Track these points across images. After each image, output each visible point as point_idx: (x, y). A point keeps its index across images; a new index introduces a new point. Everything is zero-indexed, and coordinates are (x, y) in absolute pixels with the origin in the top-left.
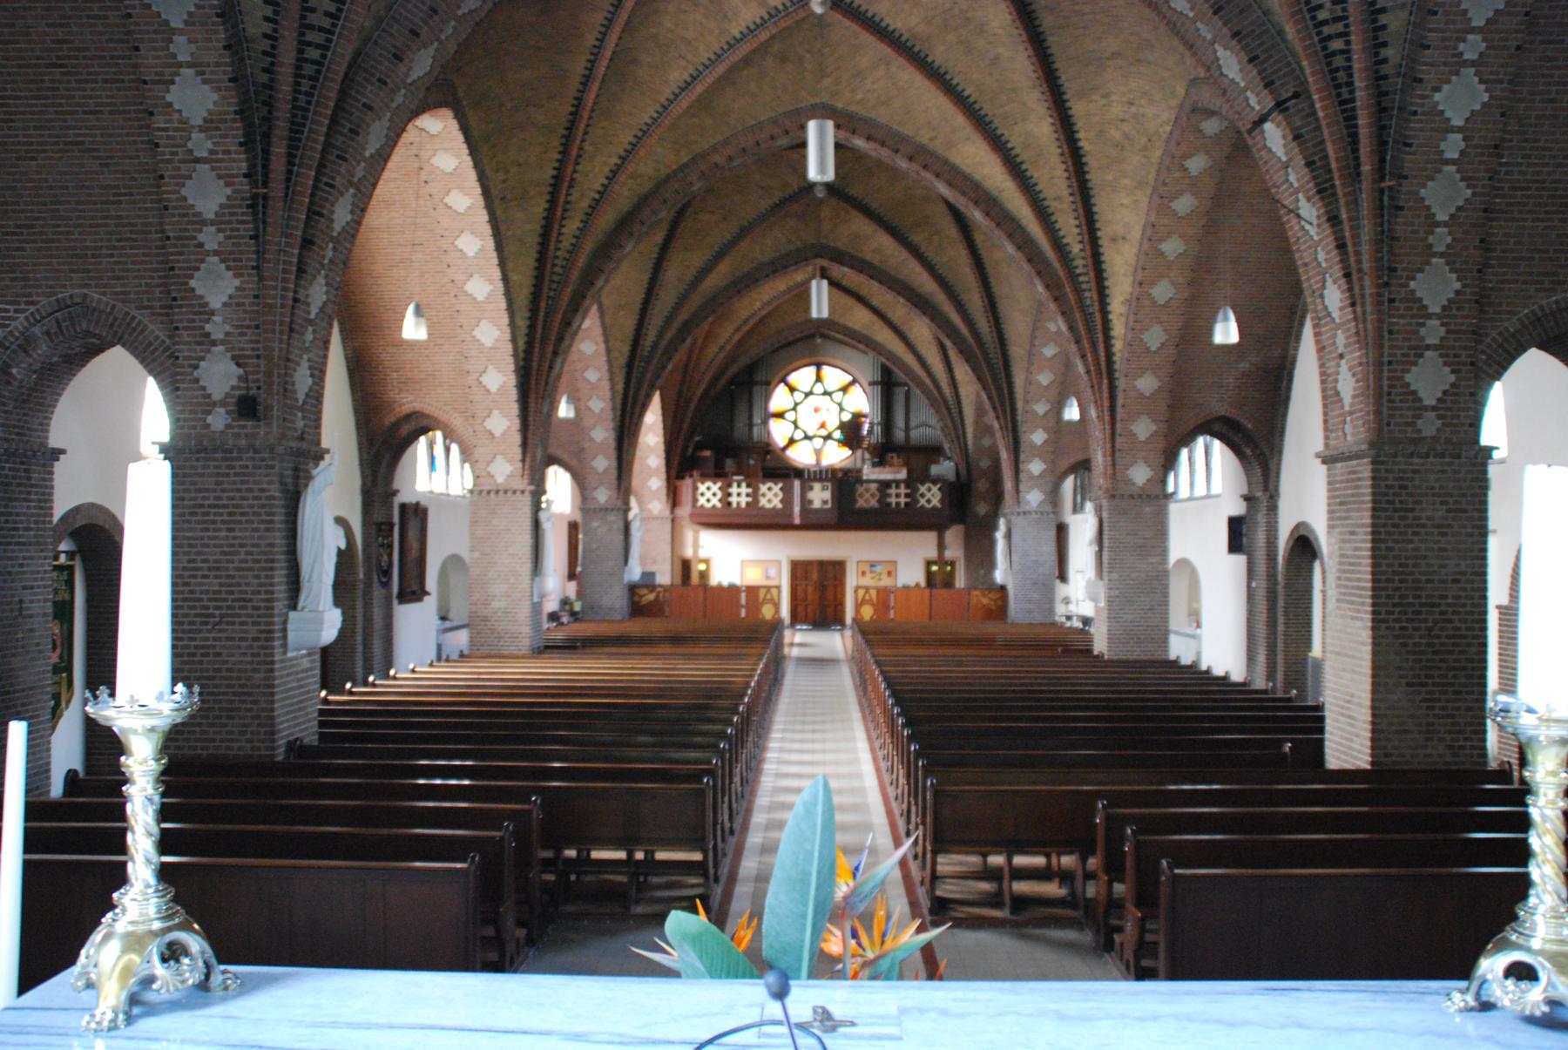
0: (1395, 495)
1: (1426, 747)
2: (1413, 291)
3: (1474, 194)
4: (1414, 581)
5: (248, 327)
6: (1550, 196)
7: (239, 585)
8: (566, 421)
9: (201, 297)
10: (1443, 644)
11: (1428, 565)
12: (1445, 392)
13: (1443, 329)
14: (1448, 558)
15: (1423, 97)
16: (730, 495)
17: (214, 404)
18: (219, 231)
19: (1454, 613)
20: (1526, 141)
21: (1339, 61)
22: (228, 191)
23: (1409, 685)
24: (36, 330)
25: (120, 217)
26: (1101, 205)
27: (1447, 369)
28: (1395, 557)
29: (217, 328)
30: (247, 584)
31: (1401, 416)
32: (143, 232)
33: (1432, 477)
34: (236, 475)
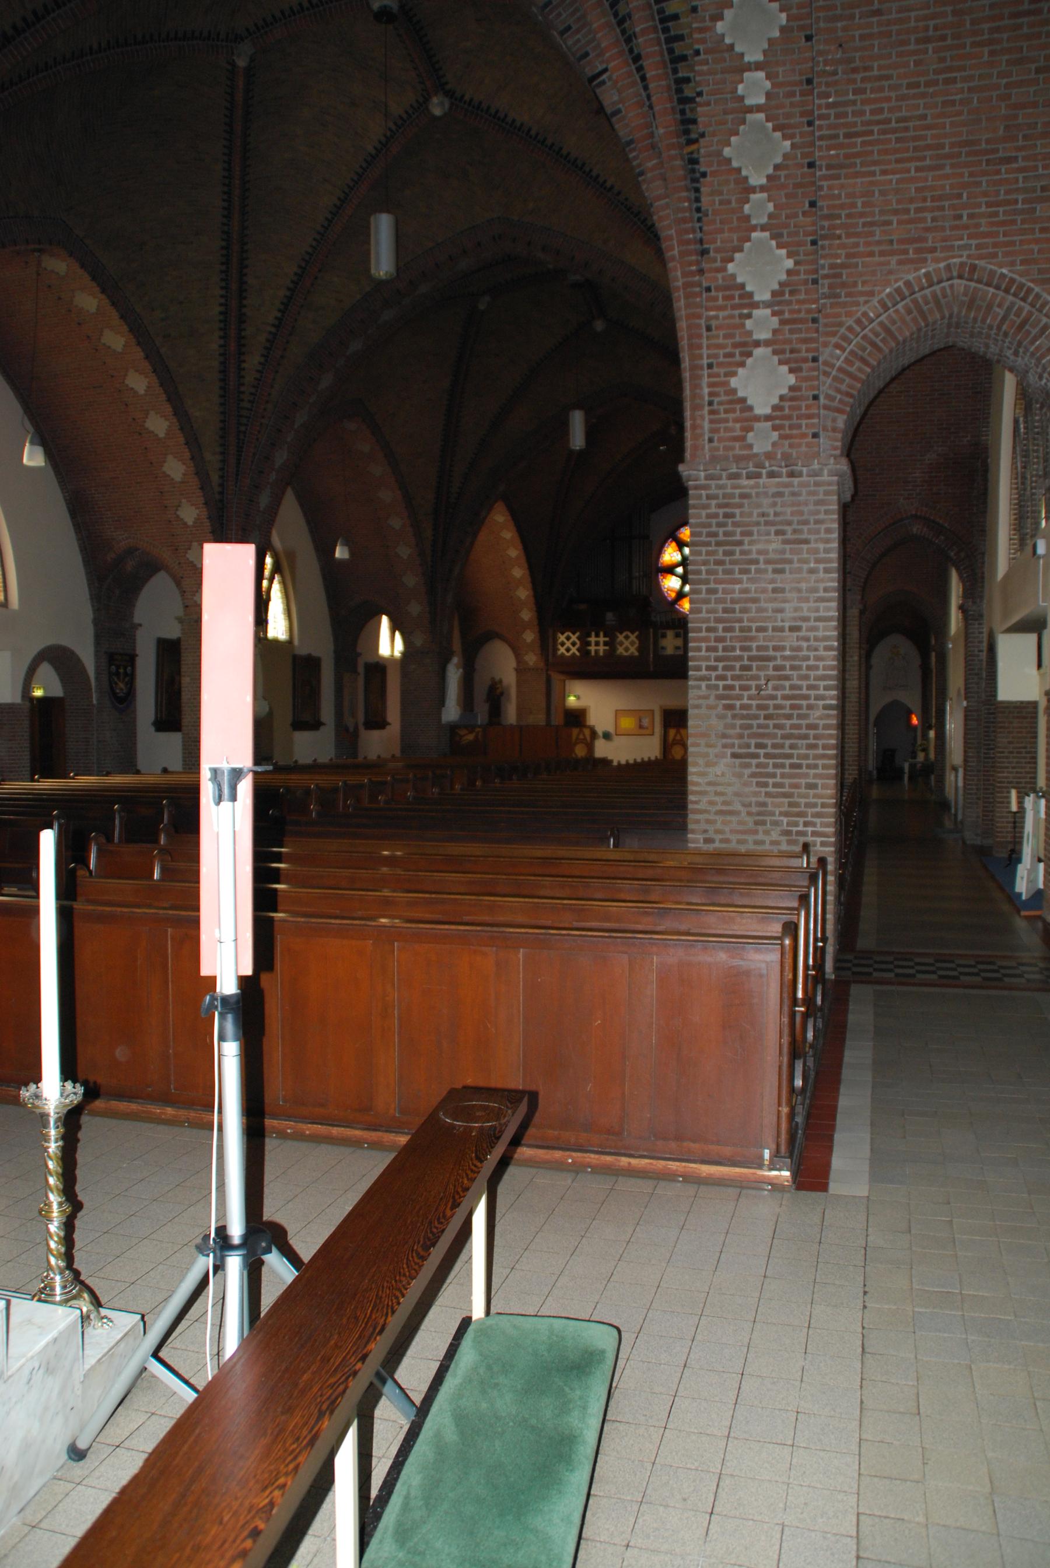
0: (719, 525)
1: (756, 832)
2: (733, 277)
3: (793, 146)
4: (742, 630)
6: (898, 140)
8: (341, 562)
10: (777, 707)
11: (760, 610)
12: (782, 398)
13: (775, 320)
14: (785, 601)
15: (701, 30)
16: (589, 644)
19: (793, 668)
20: (855, 70)
23: (734, 756)
27: (785, 368)
28: (718, 601)
31: (726, 429)
33: (766, 501)
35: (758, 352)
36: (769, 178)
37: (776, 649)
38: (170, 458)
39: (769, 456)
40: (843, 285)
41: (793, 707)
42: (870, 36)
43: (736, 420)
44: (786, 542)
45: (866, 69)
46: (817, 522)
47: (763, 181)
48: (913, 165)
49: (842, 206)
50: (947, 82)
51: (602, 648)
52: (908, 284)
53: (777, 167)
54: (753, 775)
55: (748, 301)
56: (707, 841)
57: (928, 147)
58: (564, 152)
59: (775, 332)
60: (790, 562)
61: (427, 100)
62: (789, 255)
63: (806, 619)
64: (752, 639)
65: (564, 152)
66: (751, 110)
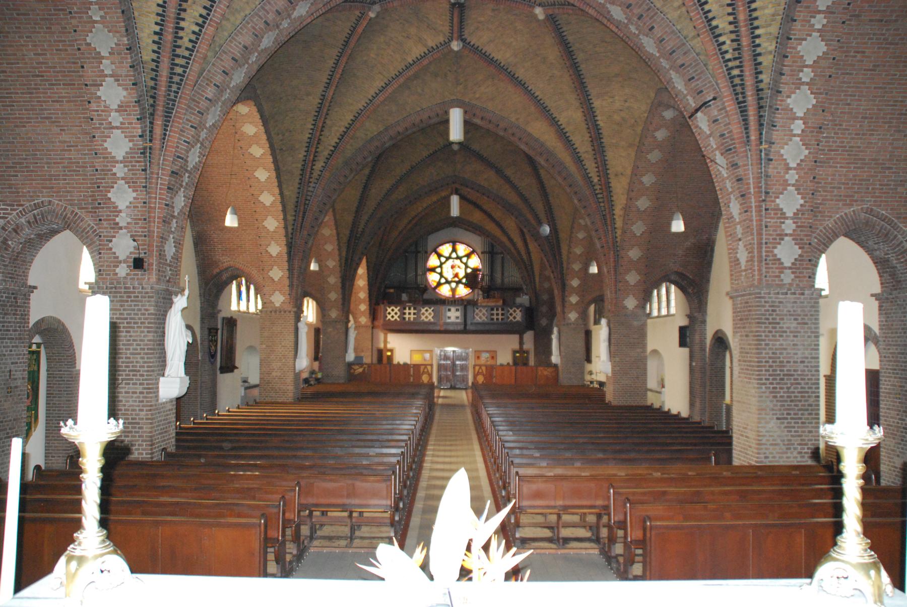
0: (770, 315)
3: (810, 153)
5: (140, 219)
7: (132, 362)
9: (114, 203)
10: (795, 397)
11: (788, 353)
12: (796, 259)
15: (781, 101)
16: (405, 314)
17: (120, 262)
18: (125, 166)
19: (802, 379)
20: (836, 125)
21: (737, 81)
22: (131, 144)
23: (778, 419)
24: (23, 220)
25: (71, 159)
26: (610, 155)
27: (797, 247)
28: (770, 349)
29: (123, 219)
30: (137, 362)
32: (83, 167)
33: (789, 305)
34: (132, 301)
35: (786, 238)
36: (798, 164)
37: (795, 371)
38: (269, 217)
39: (790, 284)
40: (820, 212)
41: (802, 397)
42: (844, 113)
43: (777, 268)
44: (799, 324)
45: (841, 125)
46: (812, 315)
47: (795, 165)
48: (853, 166)
49: (823, 179)
50: (871, 135)
51: (412, 316)
52: (846, 214)
53: (801, 161)
54: (786, 427)
55: (783, 216)
56: (766, 457)
57: (860, 159)
58: (516, 76)
59: (794, 230)
60: (799, 332)
61: (450, 41)
62: (802, 198)
63: (807, 358)
64: (784, 366)
65: (516, 76)
66: (795, 135)
